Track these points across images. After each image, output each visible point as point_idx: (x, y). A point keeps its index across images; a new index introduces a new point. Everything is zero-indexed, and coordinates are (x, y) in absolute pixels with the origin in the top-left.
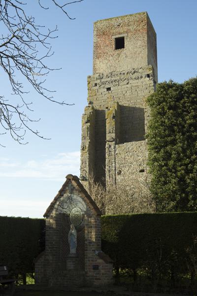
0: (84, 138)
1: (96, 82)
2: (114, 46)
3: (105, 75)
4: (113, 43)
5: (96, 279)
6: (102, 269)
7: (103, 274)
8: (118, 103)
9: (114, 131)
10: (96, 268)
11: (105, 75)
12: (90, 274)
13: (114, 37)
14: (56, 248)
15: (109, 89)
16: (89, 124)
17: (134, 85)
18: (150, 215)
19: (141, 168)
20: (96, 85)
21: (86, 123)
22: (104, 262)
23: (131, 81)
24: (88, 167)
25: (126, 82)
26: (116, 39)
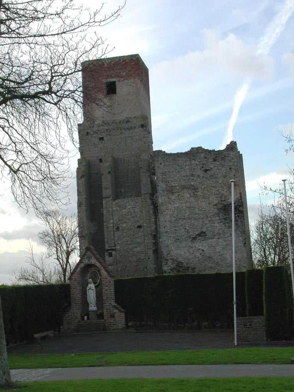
10: (112, 316)
15: (102, 139)
21: (81, 177)
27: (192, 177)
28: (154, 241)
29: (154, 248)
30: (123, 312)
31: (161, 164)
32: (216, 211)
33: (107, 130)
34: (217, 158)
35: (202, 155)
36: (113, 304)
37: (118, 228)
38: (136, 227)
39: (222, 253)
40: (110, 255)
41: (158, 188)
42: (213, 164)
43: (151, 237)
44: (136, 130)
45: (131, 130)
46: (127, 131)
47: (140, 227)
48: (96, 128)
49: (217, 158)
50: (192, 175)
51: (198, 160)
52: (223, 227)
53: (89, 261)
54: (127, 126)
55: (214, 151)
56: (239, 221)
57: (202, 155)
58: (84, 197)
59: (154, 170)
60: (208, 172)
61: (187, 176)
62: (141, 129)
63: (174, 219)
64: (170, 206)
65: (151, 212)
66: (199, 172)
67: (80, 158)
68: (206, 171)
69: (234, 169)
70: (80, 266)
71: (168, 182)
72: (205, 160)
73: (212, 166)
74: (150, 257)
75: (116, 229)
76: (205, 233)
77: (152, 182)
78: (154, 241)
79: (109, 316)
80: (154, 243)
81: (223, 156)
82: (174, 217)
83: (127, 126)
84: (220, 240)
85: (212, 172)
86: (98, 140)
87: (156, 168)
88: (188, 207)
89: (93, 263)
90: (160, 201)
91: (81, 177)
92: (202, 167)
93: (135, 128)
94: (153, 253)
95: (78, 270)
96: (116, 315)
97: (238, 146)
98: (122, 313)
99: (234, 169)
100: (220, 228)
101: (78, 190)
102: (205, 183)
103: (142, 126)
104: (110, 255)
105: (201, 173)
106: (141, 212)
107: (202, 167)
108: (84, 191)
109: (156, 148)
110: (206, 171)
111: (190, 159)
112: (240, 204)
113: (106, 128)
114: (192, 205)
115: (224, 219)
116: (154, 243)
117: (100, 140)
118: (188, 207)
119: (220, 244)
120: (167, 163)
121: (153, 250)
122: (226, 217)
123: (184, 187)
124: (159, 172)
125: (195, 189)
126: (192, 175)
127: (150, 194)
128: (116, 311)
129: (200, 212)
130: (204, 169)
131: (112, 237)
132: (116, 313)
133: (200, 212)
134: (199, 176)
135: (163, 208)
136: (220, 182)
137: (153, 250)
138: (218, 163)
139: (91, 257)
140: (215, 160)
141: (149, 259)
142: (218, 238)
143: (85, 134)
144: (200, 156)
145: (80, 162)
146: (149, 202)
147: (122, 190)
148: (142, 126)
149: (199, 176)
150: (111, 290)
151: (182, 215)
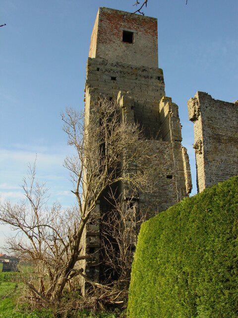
1: (99, 67)
13: (122, 29)
15: (114, 79)
20: (98, 69)
33: (121, 72)
54: (145, 73)
83: (145, 73)
93: (151, 77)
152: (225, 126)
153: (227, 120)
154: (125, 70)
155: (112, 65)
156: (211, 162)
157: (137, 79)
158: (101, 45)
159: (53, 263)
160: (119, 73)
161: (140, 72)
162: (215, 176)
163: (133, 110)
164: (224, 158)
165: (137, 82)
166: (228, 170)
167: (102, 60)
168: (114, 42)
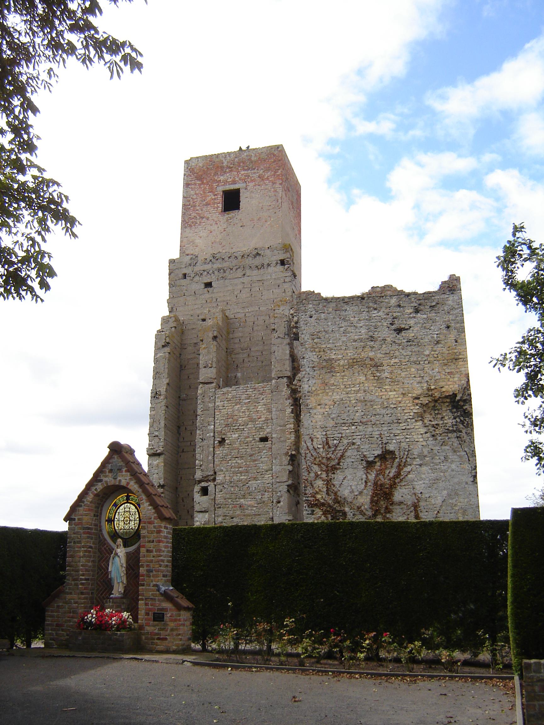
0: (157, 374)
1: (185, 271)
2: (220, 205)
3: (201, 258)
4: (220, 198)
5: (159, 639)
6: (171, 621)
7: (184, 625)
8: (223, 311)
9: (214, 365)
10: (159, 617)
11: (201, 258)
12: (148, 629)
13: (221, 189)
14: (86, 579)
15: (208, 285)
16: (167, 349)
17: (255, 279)
18: (281, 527)
19: (262, 435)
20: (185, 276)
21: (163, 346)
22: (174, 608)
23: (248, 272)
24: (163, 429)
25: (240, 273)
26: (223, 191)
27: (372, 343)
28: (290, 468)
29: (290, 482)
30: (187, 609)
31: (311, 317)
32: (417, 409)
33: (219, 270)
34: (422, 307)
35: (394, 301)
36: (163, 589)
37: (222, 442)
38: (257, 439)
39: (427, 496)
40: (205, 491)
41: (304, 362)
42: (414, 317)
43: (286, 460)
44: (271, 269)
45: (262, 270)
46: (255, 272)
47: (264, 439)
48: (198, 268)
49: (422, 307)
50: (372, 338)
51: (383, 309)
52: (431, 441)
53: (115, 479)
54: (258, 261)
55: (415, 293)
56: (464, 431)
57: (394, 301)
58: (166, 381)
59: (297, 327)
60: (403, 333)
61: (361, 340)
62: (280, 268)
63: (331, 423)
64: (326, 399)
65: (289, 410)
66: (386, 333)
67: (167, 313)
68: (399, 331)
69: (455, 328)
70: (93, 489)
71: (324, 351)
72: (398, 309)
73: (412, 322)
74: (282, 499)
75: (220, 442)
76: (392, 453)
77: (293, 358)
78: (290, 468)
79: (151, 616)
80: (290, 472)
81: (434, 304)
82: (333, 419)
83: (258, 261)
84: (424, 468)
85: (410, 334)
86: (203, 286)
87: (301, 323)
88: (361, 401)
89: (123, 483)
90: (305, 387)
91: (163, 346)
92: (392, 324)
93: (269, 265)
94: (288, 491)
95: (90, 497)
96: (168, 616)
97: (464, 286)
98: (182, 612)
99: (455, 328)
100: (424, 443)
101: (155, 369)
102: (397, 353)
103: (282, 263)
104: (205, 491)
105: (390, 336)
106: (270, 411)
107: (392, 324)
108: (167, 371)
109: (305, 287)
110: (399, 331)
111: (368, 307)
112: (465, 398)
113: (217, 265)
114: (369, 397)
115: (433, 426)
116: (290, 472)
117: (206, 287)
118: (361, 401)
119: (423, 476)
120: (323, 316)
121: (288, 486)
122: (436, 422)
123: (354, 363)
124: (305, 336)
125: (376, 366)
126: (372, 338)
127: (288, 377)
128: (167, 605)
129: (383, 411)
130: (393, 327)
131: (210, 458)
132: (166, 610)
133: (383, 411)
134: (384, 340)
135: (312, 401)
136: (427, 353)
137: (288, 486)
138: (425, 316)
139: (120, 470)
140: (417, 311)
141: (279, 502)
142: (420, 465)
143: (181, 276)
144: (389, 303)
145: (165, 320)
146: (286, 392)
147: (239, 375)
148: (282, 263)
149: (384, 340)
150: (160, 551)
151: (348, 416)
152: (343, 342)
153: (349, 329)
154: (225, 265)
155: (205, 262)
156: (315, 408)
157: (244, 275)
158: (188, 230)
159: (75, 38)
160: (216, 272)
161: (249, 261)
162: (322, 430)
163: (215, 343)
164: (337, 397)
165: (246, 280)
166: (344, 416)
167: (189, 257)
168: (208, 219)
